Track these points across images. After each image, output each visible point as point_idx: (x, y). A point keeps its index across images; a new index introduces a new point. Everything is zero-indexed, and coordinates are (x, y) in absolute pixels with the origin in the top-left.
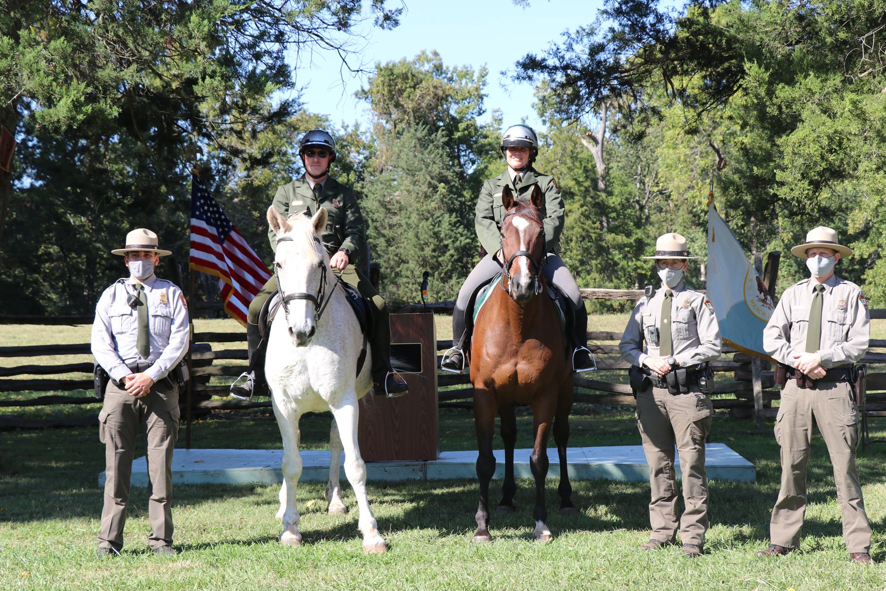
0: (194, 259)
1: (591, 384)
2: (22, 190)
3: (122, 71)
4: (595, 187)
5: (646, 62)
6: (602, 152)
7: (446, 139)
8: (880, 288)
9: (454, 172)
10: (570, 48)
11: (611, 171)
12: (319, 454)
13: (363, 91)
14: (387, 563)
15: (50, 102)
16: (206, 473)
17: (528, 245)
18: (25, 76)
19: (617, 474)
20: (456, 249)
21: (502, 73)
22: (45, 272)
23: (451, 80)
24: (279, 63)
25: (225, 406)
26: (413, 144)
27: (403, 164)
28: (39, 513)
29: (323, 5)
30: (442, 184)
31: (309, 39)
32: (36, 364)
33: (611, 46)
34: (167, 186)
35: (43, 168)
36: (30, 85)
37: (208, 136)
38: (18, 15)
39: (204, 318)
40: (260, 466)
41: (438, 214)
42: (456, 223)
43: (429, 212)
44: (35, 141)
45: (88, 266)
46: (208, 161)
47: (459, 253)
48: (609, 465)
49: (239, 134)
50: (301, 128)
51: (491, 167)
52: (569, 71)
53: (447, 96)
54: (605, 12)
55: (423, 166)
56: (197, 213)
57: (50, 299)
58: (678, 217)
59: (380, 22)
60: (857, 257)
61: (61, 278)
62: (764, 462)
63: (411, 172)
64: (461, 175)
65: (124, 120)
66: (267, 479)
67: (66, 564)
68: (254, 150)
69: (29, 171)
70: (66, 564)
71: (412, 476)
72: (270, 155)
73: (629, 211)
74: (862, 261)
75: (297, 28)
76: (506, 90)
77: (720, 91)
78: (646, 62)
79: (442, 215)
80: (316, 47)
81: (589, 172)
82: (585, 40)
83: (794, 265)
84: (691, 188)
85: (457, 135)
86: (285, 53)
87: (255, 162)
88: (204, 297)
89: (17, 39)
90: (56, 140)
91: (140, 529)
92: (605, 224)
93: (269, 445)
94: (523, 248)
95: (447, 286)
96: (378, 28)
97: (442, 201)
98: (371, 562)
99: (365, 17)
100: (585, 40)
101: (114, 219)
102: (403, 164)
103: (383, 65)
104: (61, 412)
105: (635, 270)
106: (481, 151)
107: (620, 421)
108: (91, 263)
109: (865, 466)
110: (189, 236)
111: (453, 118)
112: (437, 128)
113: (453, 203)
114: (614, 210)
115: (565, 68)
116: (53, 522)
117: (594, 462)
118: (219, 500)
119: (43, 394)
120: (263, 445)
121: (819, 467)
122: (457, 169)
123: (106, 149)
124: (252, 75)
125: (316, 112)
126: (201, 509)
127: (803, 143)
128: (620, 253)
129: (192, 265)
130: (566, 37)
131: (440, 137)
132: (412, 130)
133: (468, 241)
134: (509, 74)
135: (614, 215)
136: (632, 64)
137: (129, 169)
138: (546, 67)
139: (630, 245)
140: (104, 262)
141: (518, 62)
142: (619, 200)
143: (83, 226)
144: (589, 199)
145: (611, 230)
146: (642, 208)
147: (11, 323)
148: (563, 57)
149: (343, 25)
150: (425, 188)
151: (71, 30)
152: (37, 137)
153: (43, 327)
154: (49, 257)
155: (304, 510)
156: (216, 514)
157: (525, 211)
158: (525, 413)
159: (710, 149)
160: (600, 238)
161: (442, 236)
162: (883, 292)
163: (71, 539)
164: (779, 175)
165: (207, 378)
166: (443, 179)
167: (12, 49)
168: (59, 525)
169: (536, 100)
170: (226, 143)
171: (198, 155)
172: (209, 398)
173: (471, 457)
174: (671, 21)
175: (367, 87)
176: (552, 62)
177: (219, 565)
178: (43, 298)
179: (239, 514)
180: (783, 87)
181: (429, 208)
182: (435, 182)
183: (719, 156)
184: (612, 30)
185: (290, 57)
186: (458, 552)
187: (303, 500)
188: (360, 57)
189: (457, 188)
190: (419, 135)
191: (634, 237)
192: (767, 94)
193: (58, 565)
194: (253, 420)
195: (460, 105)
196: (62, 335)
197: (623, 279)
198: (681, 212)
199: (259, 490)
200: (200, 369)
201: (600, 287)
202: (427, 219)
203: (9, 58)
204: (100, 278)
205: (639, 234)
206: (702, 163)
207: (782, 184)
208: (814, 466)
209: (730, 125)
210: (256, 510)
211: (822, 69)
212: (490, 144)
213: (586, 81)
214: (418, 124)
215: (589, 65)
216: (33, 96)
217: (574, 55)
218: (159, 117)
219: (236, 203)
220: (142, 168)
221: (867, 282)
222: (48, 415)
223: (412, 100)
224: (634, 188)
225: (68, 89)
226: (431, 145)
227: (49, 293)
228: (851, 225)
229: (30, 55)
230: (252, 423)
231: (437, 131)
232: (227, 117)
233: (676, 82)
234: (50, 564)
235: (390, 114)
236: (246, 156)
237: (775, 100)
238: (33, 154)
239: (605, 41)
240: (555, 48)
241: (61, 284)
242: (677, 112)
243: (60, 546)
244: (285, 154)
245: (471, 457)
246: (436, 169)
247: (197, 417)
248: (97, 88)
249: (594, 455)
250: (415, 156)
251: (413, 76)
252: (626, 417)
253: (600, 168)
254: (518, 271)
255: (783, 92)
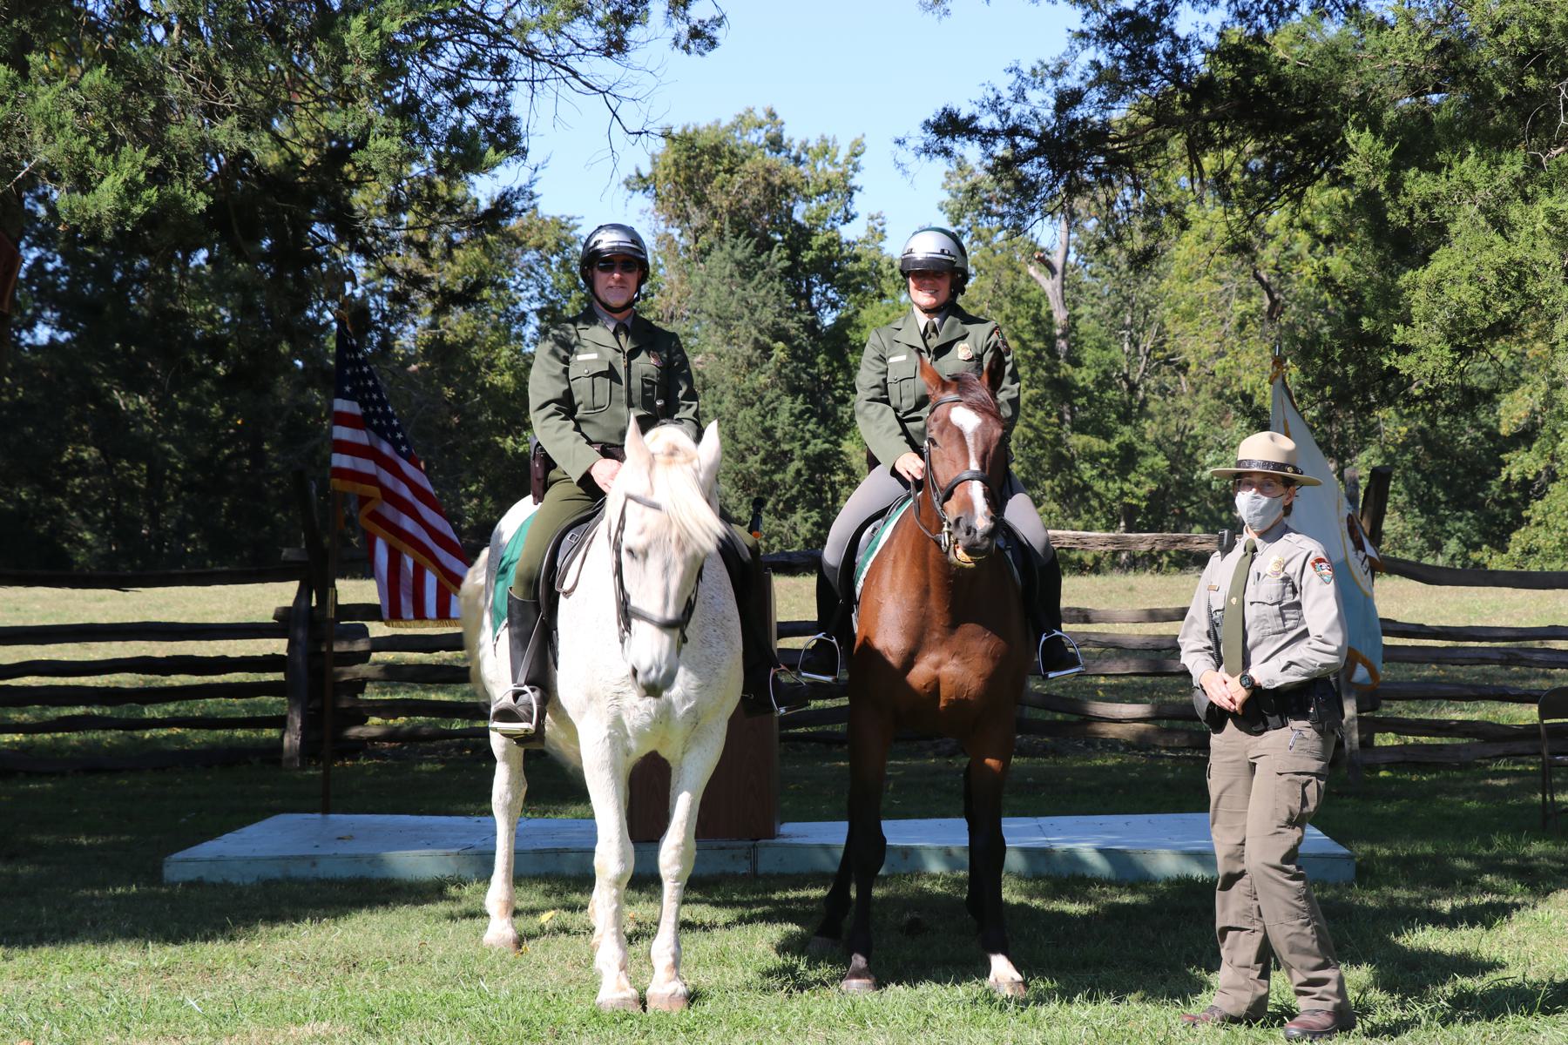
0: (341, 473)
1: (1049, 702)
2: (34, 348)
3: (212, 127)
4: (1052, 351)
5: (1157, 124)
6: (1063, 288)
7: (787, 263)
8: (1555, 533)
9: (800, 321)
10: (1020, 96)
11: (1078, 323)
12: (556, 825)
13: (640, 176)
14: (688, 1031)
15: (83, 184)
16: (356, 858)
17: (983, 459)
18: (37, 137)
19: (1099, 864)
20: (806, 458)
21: (898, 142)
22: (73, 493)
23: (798, 160)
24: (499, 114)
25: (392, 735)
26: (727, 272)
27: (709, 306)
28: (53, 931)
29: (579, 11)
30: (781, 344)
31: (552, 75)
32: (54, 657)
33: (1094, 95)
34: (291, 341)
35: (70, 310)
36: (44, 154)
37: (366, 252)
38: (26, 27)
39: (354, 577)
40: (455, 846)
41: (770, 395)
42: (802, 413)
43: (754, 391)
44: (58, 262)
45: (150, 482)
46: (364, 297)
47: (809, 468)
48: (1087, 850)
49: (423, 249)
50: (531, 242)
51: (865, 314)
52: (1018, 139)
53: (789, 187)
54: (1083, 35)
55: (746, 312)
56: (348, 389)
57: (82, 542)
58: (1197, 404)
59: (683, 42)
60: (1516, 477)
61: (103, 503)
62: (1366, 848)
63: (723, 321)
64: (811, 327)
65: (217, 217)
66: (466, 873)
67: (101, 1028)
68: (448, 275)
69: (48, 314)
70: (101, 1028)
71: (730, 868)
72: (478, 286)
73: (1110, 394)
74: (1525, 484)
75: (531, 53)
76: (905, 173)
77: (1285, 180)
78: (1157, 124)
79: (778, 398)
80: (564, 90)
81: (1042, 324)
82: (1049, 83)
83: (1405, 492)
84: (1221, 354)
85: (807, 256)
86: (510, 96)
87: (447, 300)
88: (354, 540)
89: (23, 69)
90: (96, 260)
91: (237, 962)
92: (1068, 417)
93: (472, 807)
94: (974, 465)
95: (786, 524)
96: (678, 52)
97: (779, 372)
98: (658, 1028)
99: (654, 33)
100: (1049, 83)
101: (196, 401)
102: (709, 306)
103: (677, 131)
104: (97, 743)
105: (1119, 498)
106: (849, 285)
107: (1102, 769)
108: (154, 477)
109: (1551, 857)
110: (330, 431)
111: (799, 227)
112: (770, 245)
113: (798, 377)
114: (1084, 392)
115: (1012, 132)
116: (79, 948)
117: (1061, 845)
118: (381, 909)
119: (66, 712)
120: (460, 807)
121: (1468, 858)
122: (805, 317)
123: (183, 276)
124: (455, 136)
125: (557, 214)
126: (347, 925)
127: (1455, 274)
128: (1093, 468)
129: (336, 483)
130: (1013, 76)
131: (778, 259)
132: (727, 247)
133: (827, 446)
134: (911, 143)
135: (1083, 400)
136: (1132, 126)
137: (223, 311)
138: (976, 131)
139: (1110, 455)
140: (178, 477)
141: (927, 122)
142: (1093, 375)
143: (140, 411)
144: (1041, 372)
145: (1079, 428)
146: (1133, 388)
147: (11, 585)
148: (1007, 113)
149: (615, 47)
150: (747, 349)
151: (122, 53)
152: (61, 253)
153: (67, 591)
154: (81, 467)
155: (534, 928)
156: (377, 936)
157: (972, 397)
158: (930, 753)
159: (1255, 285)
160: (1058, 440)
161: (779, 434)
162: (1561, 540)
163: (111, 979)
164: (1400, 334)
165: (359, 685)
166: (779, 334)
167: (14, 87)
168: (93, 953)
169: (946, 197)
170: (397, 264)
171: (348, 286)
172: (362, 721)
173: (835, 834)
174: (1203, 50)
175: (646, 171)
176: (987, 121)
177: (380, 1031)
178: (70, 540)
179: (417, 935)
180: (1418, 175)
181: (756, 385)
182: (765, 339)
183: (1271, 296)
184: (1096, 65)
185: (519, 102)
186: (817, 1011)
187: (534, 912)
188: (645, 108)
189: (805, 350)
190: (738, 255)
191: (1118, 439)
192: (1387, 188)
193: (87, 1028)
194: (442, 762)
195: (814, 203)
196: (102, 605)
197: (1098, 514)
198: (1202, 396)
199: (453, 891)
200: (347, 669)
201: (1058, 527)
202: (752, 405)
203: (9, 104)
204: (171, 504)
205: (1126, 433)
206: (1239, 307)
207: (1405, 350)
208: (1459, 855)
209: (1304, 241)
210: (450, 928)
211: (1496, 142)
212: (862, 273)
213: (1061, 155)
214: (737, 237)
215: (1054, 129)
216: (55, 178)
217: (1027, 110)
218: (281, 214)
219: (414, 372)
220: (246, 308)
221: (1533, 522)
222: (74, 749)
223: (728, 193)
224: (1119, 352)
225: (116, 159)
226: (760, 273)
227: (81, 530)
228: (1504, 421)
229: (45, 97)
230: (439, 767)
231: (770, 249)
232: (404, 218)
233: (1209, 162)
234: (72, 1026)
235: (688, 219)
236: (435, 287)
237: (1402, 200)
238: (55, 285)
239: (1083, 84)
240: (992, 97)
241: (101, 515)
242: (1211, 218)
243: (91, 993)
244: (504, 286)
245: (835, 834)
246: (767, 316)
247: (342, 755)
248: (167, 159)
249: (1060, 831)
250: (732, 293)
251: (732, 153)
252: (1110, 762)
253: (1060, 316)
254: (968, 505)
255: (1419, 184)
